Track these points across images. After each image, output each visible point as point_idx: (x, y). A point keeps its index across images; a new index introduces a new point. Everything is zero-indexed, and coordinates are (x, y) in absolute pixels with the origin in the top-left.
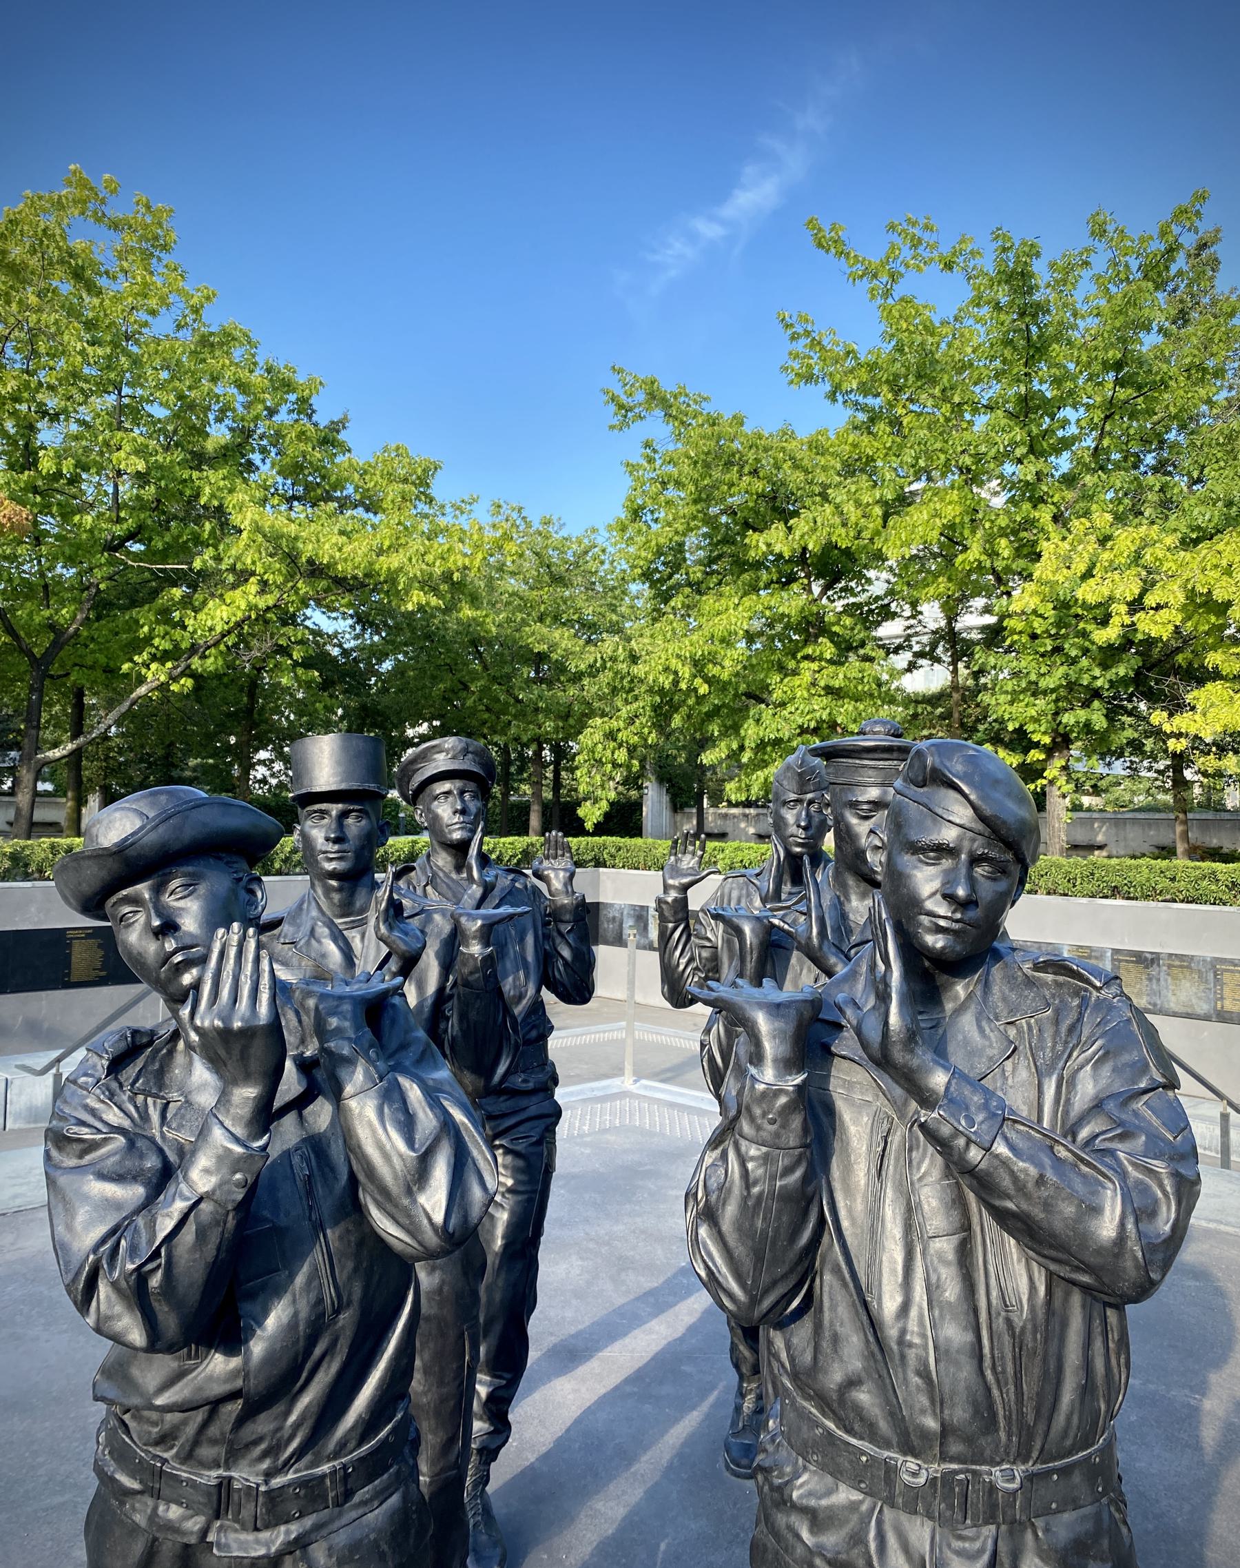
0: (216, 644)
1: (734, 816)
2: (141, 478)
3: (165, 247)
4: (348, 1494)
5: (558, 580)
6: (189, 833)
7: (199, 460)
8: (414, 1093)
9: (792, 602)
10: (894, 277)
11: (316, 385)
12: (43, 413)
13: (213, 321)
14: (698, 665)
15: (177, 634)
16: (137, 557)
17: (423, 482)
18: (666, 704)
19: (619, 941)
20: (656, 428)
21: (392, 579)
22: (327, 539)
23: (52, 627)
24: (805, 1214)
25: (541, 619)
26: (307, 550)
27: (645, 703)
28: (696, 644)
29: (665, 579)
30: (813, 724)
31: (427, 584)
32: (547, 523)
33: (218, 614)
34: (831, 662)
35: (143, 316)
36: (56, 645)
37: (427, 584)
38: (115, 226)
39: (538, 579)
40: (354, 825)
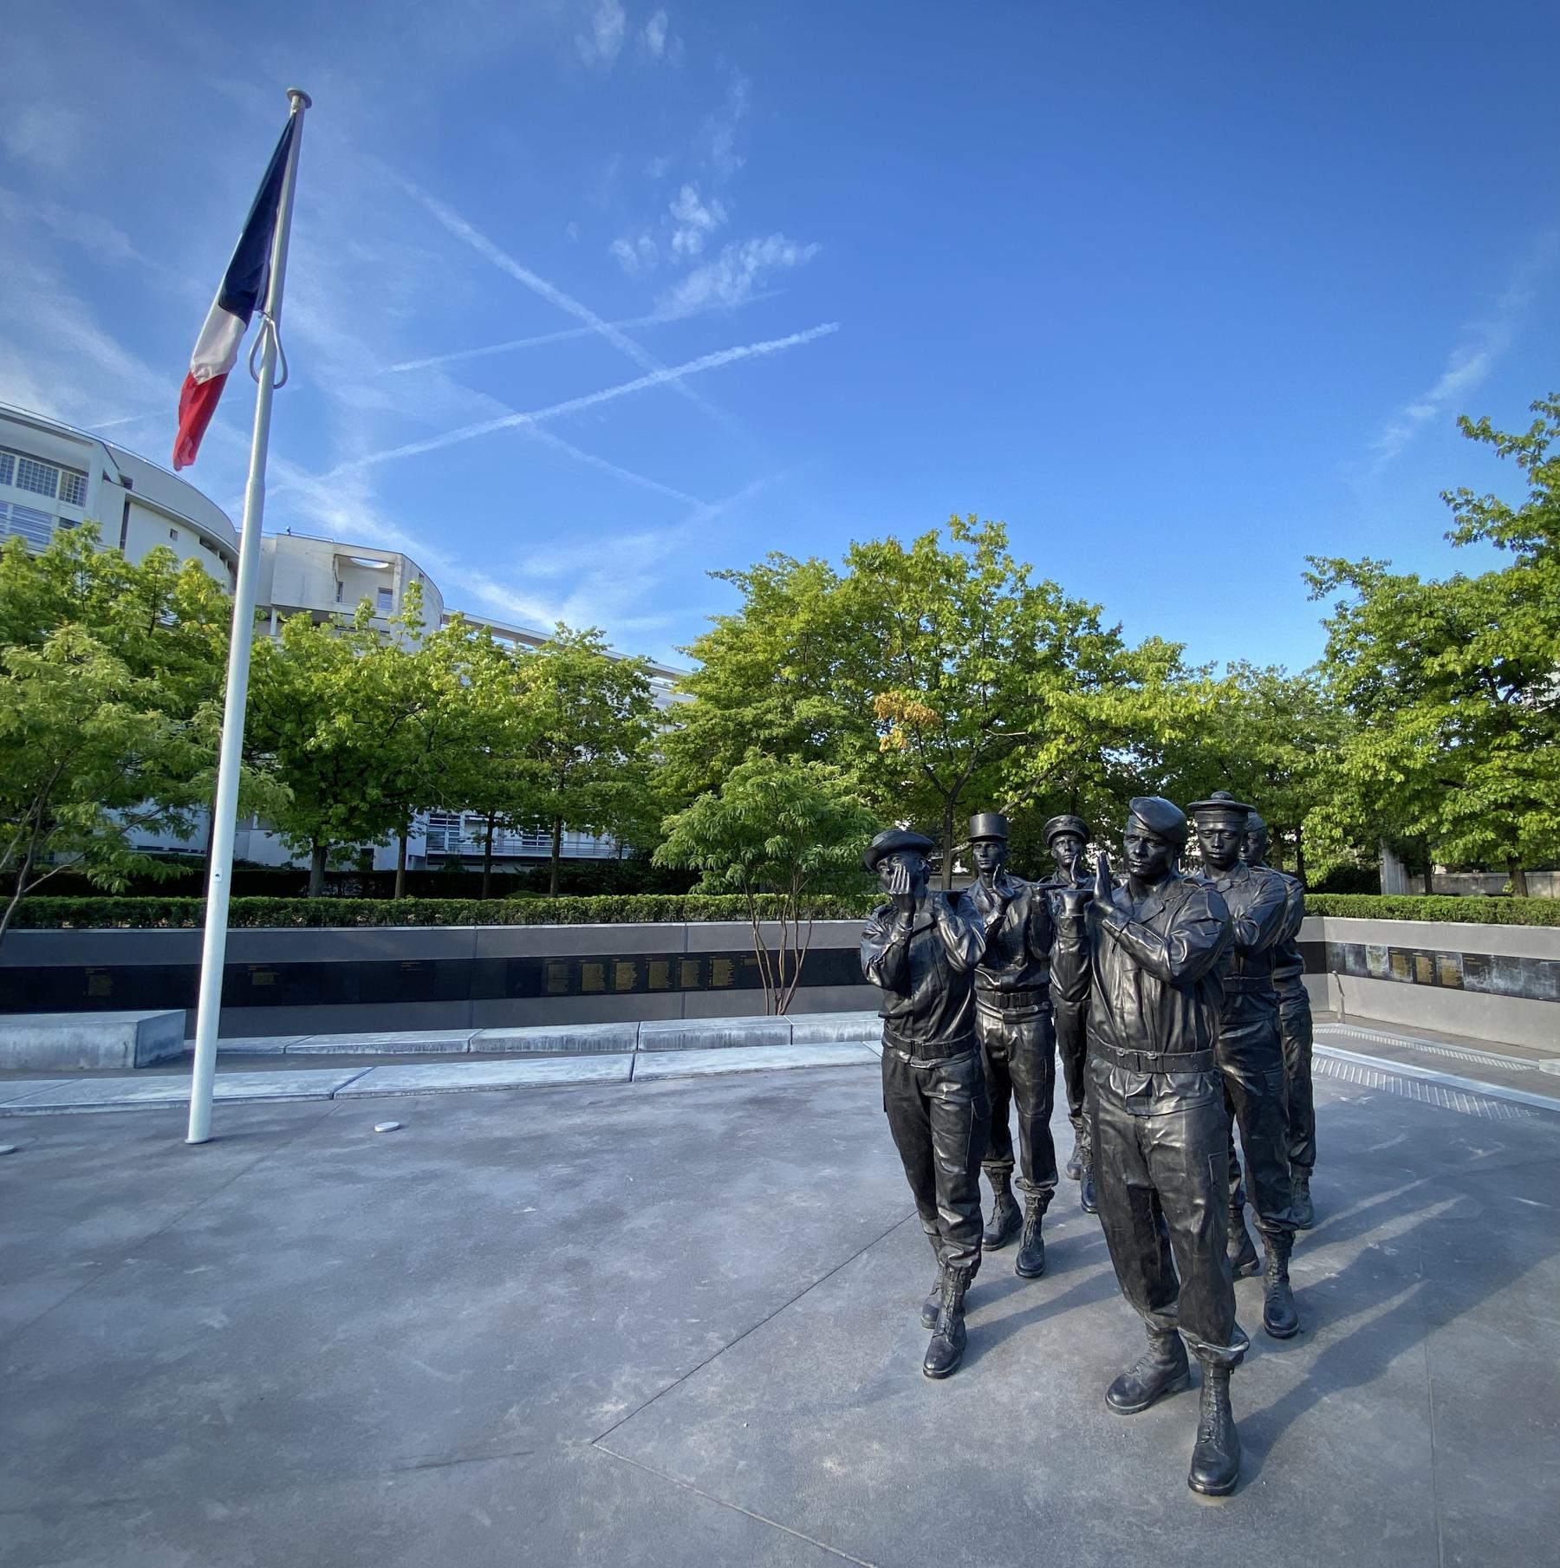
0: (1045, 777)
1: (1465, 880)
2: (996, 683)
3: (1003, 547)
4: (951, 1055)
5: (1281, 711)
6: (898, 843)
7: (1031, 667)
8: (960, 921)
9: (1478, 709)
10: (1541, 446)
11: (1098, 609)
12: (943, 655)
13: (1033, 582)
14: (1393, 761)
15: (1023, 774)
16: (1001, 730)
17: (1173, 658)
18: (1370, 792)
19: (1343, 970)
20: (1348, 593)
21: (1150, 722)
22: (1106, 705)
23: (955, 775)
24: (1082, 962)
25: (1270, 741)
26: (1093, 713)
27: (1353, 794)
28: (1391, 745)
29: (1365, 698)
30: (1506, 800)
31: (1174, 724)
32: (1270, 670)
33: (1045, 758)
34: (1517, 748)
35: (993, 589)
36: (958, 786)
37: (1174, 724)
38: (974, 541)
39: (1267, 711)
40: (991, 851)
